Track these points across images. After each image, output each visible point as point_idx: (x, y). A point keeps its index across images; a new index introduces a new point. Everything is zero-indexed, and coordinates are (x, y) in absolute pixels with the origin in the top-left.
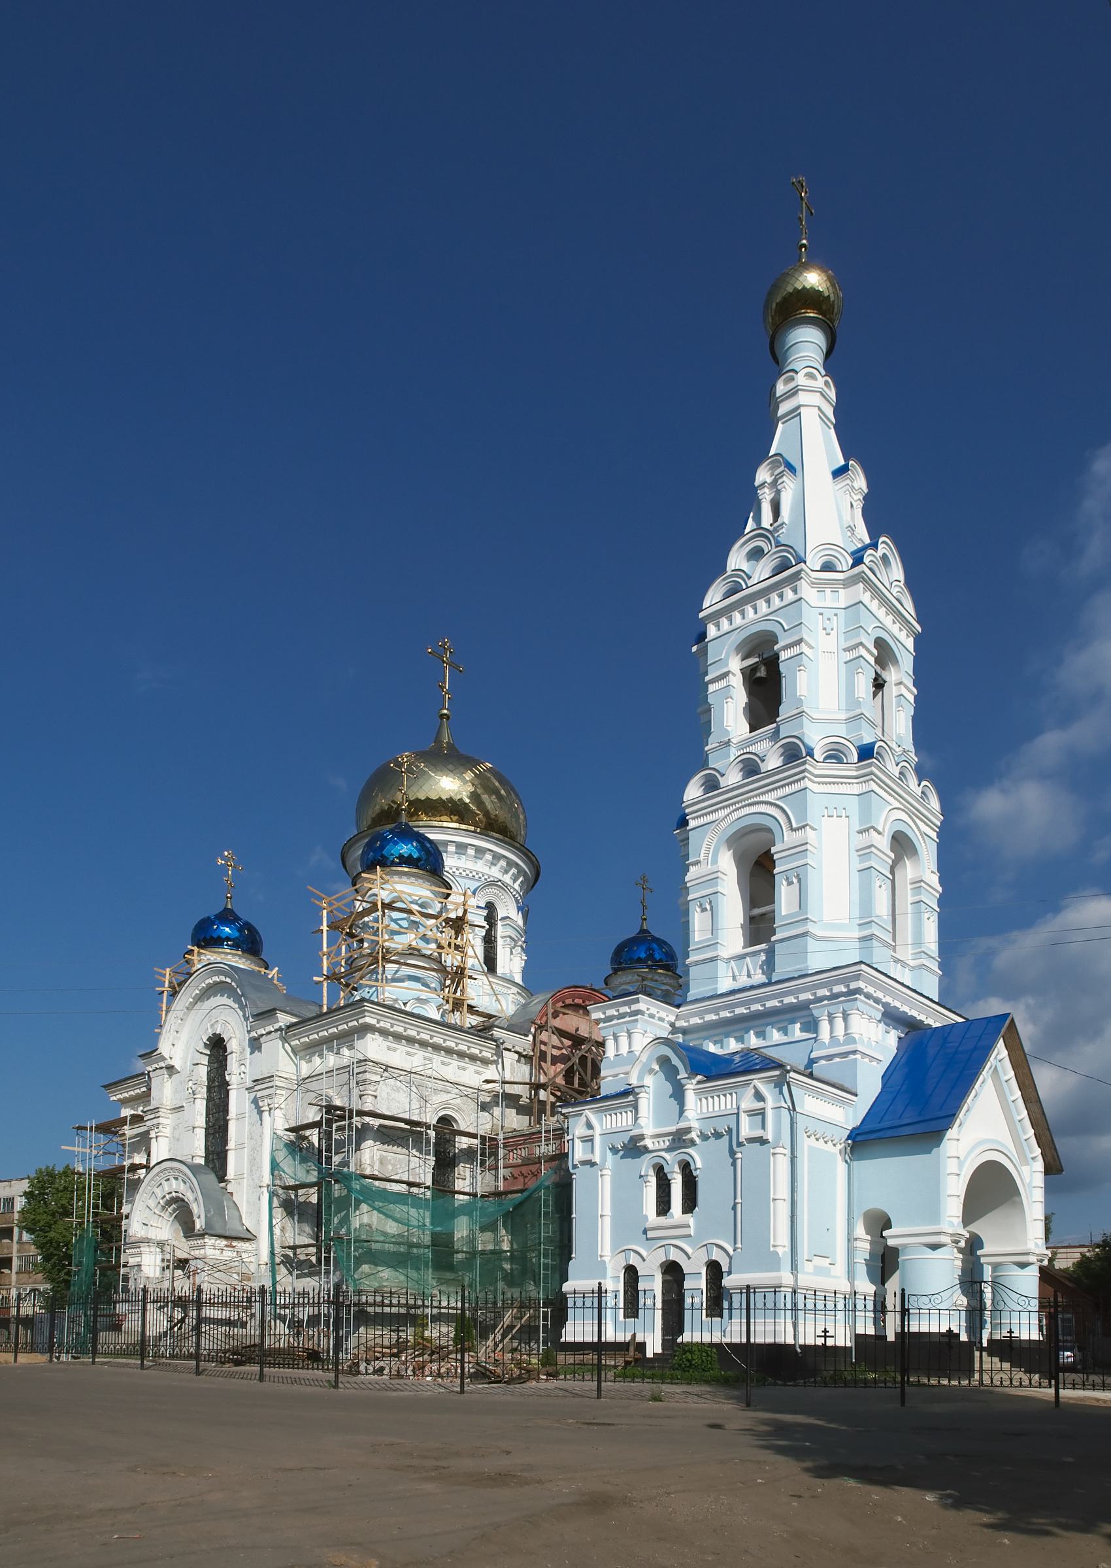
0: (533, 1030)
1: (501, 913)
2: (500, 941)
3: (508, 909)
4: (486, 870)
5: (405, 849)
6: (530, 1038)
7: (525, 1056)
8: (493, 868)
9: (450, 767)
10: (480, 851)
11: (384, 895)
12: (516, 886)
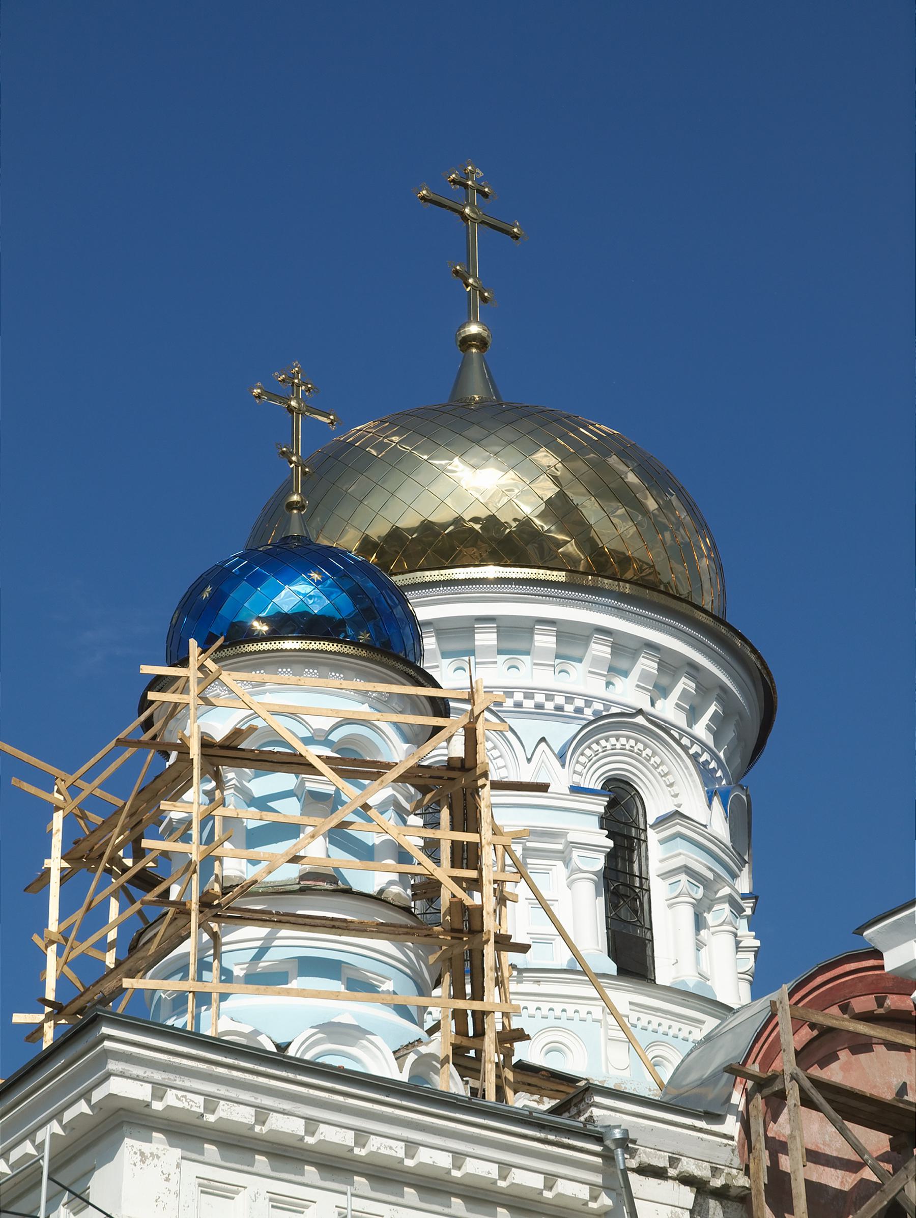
0: (738, 1098)
1: (655, 805)
2: (659, 892)
3: (675, 791)
4: (596, 687)
5: (296, 594)
6: (732, 1126)
7: (722, 1194)
8: (618, 681)
9: (474, 432)
10: (572, 639)
11: (219, 726)
12: (701, 730)
